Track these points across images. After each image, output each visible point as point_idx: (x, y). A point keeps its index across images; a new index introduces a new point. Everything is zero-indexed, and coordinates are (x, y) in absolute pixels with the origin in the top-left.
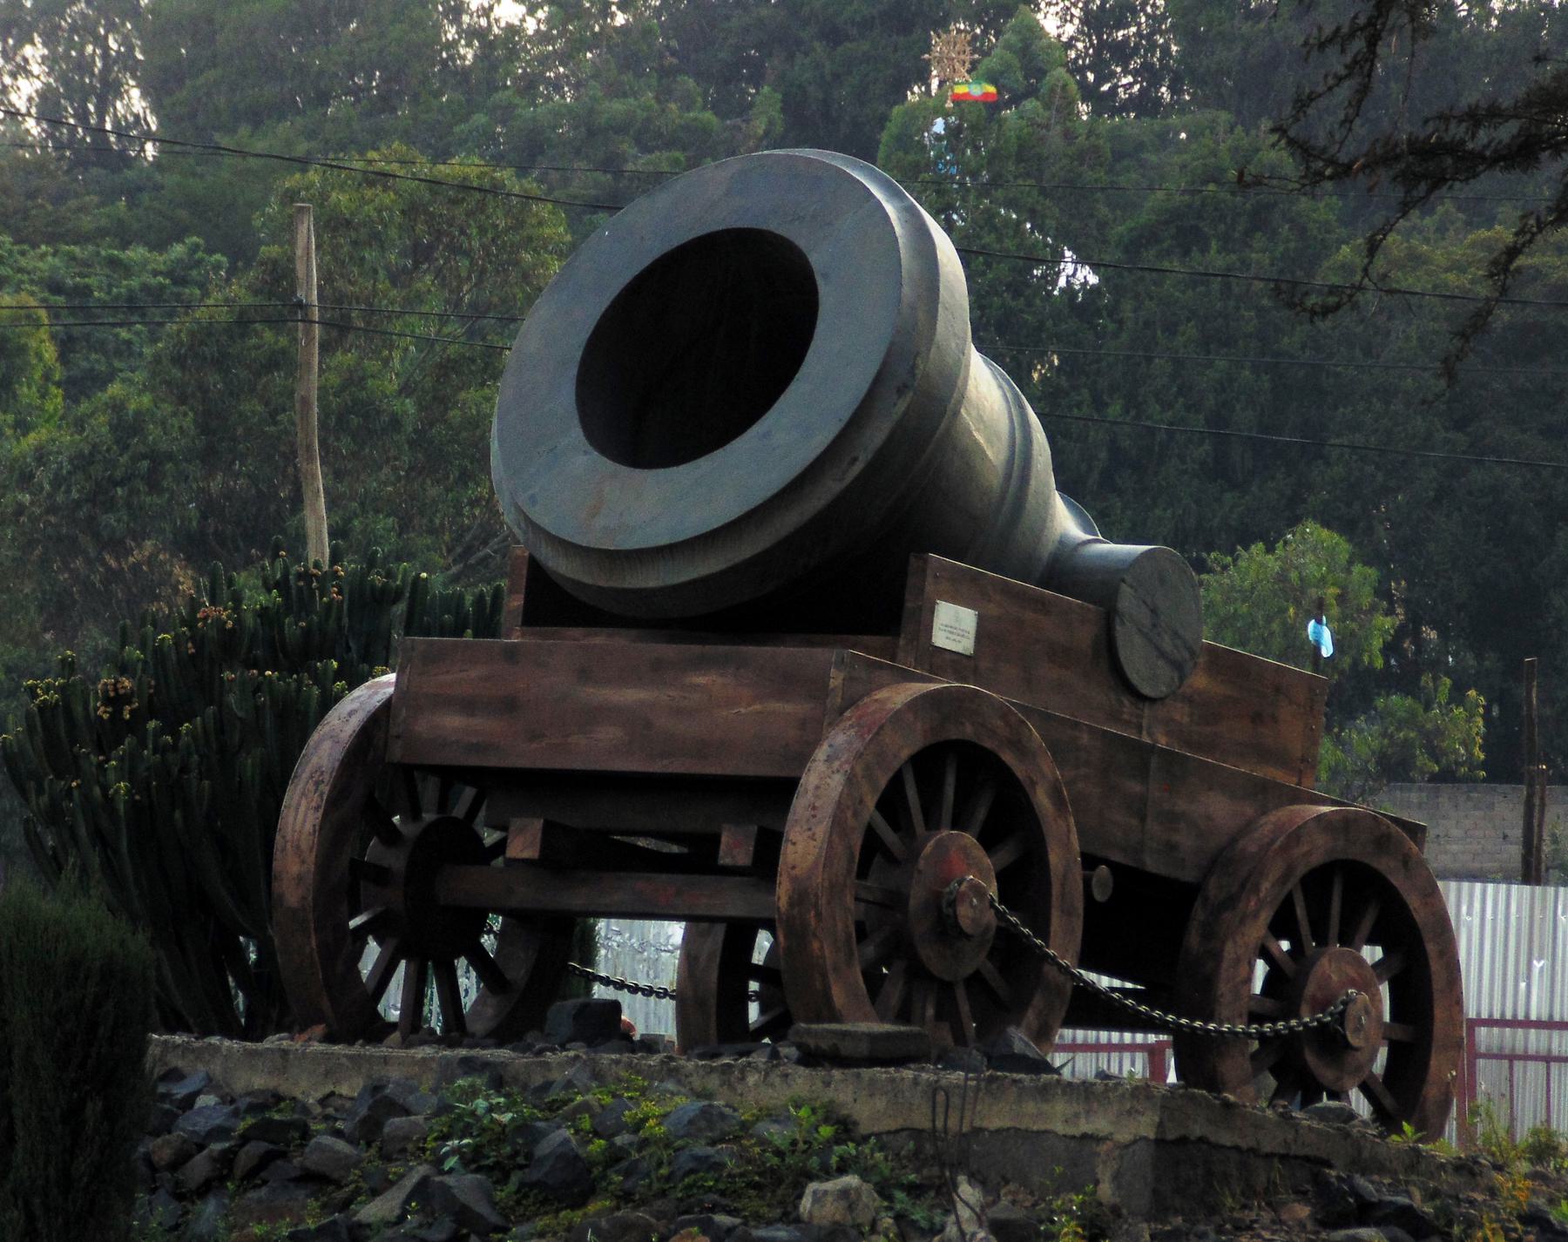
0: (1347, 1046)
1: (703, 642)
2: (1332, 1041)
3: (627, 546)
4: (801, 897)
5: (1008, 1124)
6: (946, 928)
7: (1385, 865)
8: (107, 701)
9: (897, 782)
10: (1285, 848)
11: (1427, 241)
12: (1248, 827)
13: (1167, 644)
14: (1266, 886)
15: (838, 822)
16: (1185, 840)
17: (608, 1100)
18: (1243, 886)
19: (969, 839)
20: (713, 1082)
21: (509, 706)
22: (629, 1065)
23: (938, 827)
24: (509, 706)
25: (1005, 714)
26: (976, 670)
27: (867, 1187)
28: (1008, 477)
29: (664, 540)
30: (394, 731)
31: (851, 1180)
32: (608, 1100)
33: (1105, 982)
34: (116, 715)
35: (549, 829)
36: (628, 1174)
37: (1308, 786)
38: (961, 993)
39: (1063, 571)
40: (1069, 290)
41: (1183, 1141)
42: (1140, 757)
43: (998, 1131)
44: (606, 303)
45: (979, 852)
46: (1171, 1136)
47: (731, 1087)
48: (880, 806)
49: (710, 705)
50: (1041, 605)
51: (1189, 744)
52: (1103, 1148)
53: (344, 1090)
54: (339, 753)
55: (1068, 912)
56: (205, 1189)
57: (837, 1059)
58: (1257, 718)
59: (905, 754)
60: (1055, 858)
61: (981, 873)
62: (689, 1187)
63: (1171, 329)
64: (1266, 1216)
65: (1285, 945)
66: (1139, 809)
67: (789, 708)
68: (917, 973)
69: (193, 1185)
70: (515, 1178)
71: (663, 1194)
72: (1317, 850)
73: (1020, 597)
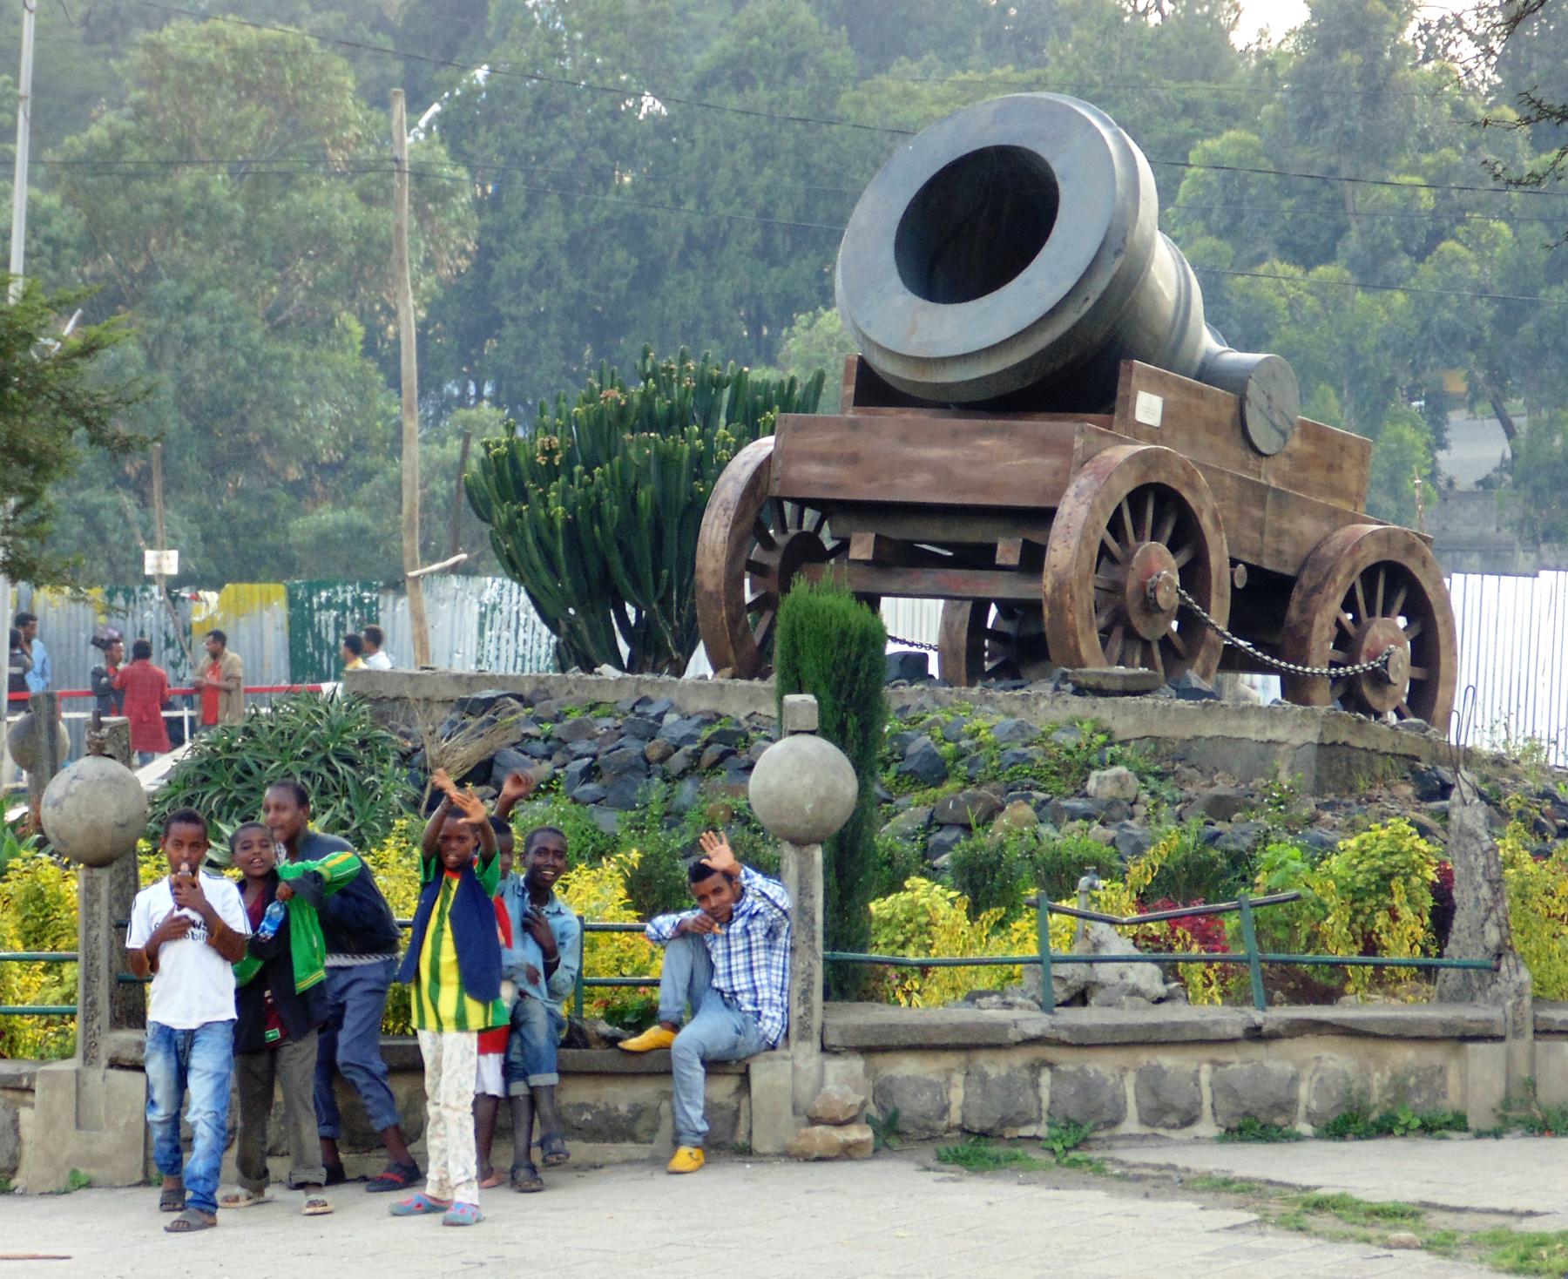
0: (1389, 682)
1: (986, 418)
2: (1379, 678)
3: (935, 355)
4: (1060, 586)
5: (1217, 733)
6: (1150, 606)
7: (1413, 565)
8: (545, 453)
9: (1119, 510)
10: (1352, 553)
11: (915, 81)
12: (1325, 539)
13: (1277, 419)
14: (1340, 578)
15: (1084, 537)
16: (1287, 547)
17: (950, 718)
18: (1326, 578)
19: (1162, 547)
20: (1017, 706)
21: (853, 459)
22: (959, 695)
23: (1142, 539)
24: (853, 459)
25: (1185, 466)
26: (1161, 437)
27: (1131, 774)
28: (1177, 308)
29: (960, 352)
30: (774, 475)
31: (1121, 769)
32: (950, 718)
33: (1241, 642)
34: (550, 462)
35: (879, 539)
36: (970, 765)
37: (1361, 511)
38: (1156, 648)
39: (1208, 373)
40: (648, 116)
41: (1334, 744)
42: (1260, 493)
43: (1210, 739)
44: (913, 195)
45: (1167, 554)
46: (1327, 742)
47: (1029, 710)
48: (1109, 527)
49: (993, 461)
50: (1201, 394)
51: (1290, 485)
52: (1282, 749)
53: (763, 710)
54: (740, 490)
55: (1221, 595)
56: (683, 775)
57: (1099, 692)
58: (1330, 468)
59: (1125, 492)
60: (1214, 560)
61: (1169, 569)
62: (1012, 774)
63: (731, 147)
64: (1385, 793)
65: (1350, 616)
66: (1259, 527)
67: (1047, 461)
68: (1130, 634)
69: (674, 772)
70: (894, 767)
71: (995, 778)
72: (1370, 556)
73: (1188, 388)
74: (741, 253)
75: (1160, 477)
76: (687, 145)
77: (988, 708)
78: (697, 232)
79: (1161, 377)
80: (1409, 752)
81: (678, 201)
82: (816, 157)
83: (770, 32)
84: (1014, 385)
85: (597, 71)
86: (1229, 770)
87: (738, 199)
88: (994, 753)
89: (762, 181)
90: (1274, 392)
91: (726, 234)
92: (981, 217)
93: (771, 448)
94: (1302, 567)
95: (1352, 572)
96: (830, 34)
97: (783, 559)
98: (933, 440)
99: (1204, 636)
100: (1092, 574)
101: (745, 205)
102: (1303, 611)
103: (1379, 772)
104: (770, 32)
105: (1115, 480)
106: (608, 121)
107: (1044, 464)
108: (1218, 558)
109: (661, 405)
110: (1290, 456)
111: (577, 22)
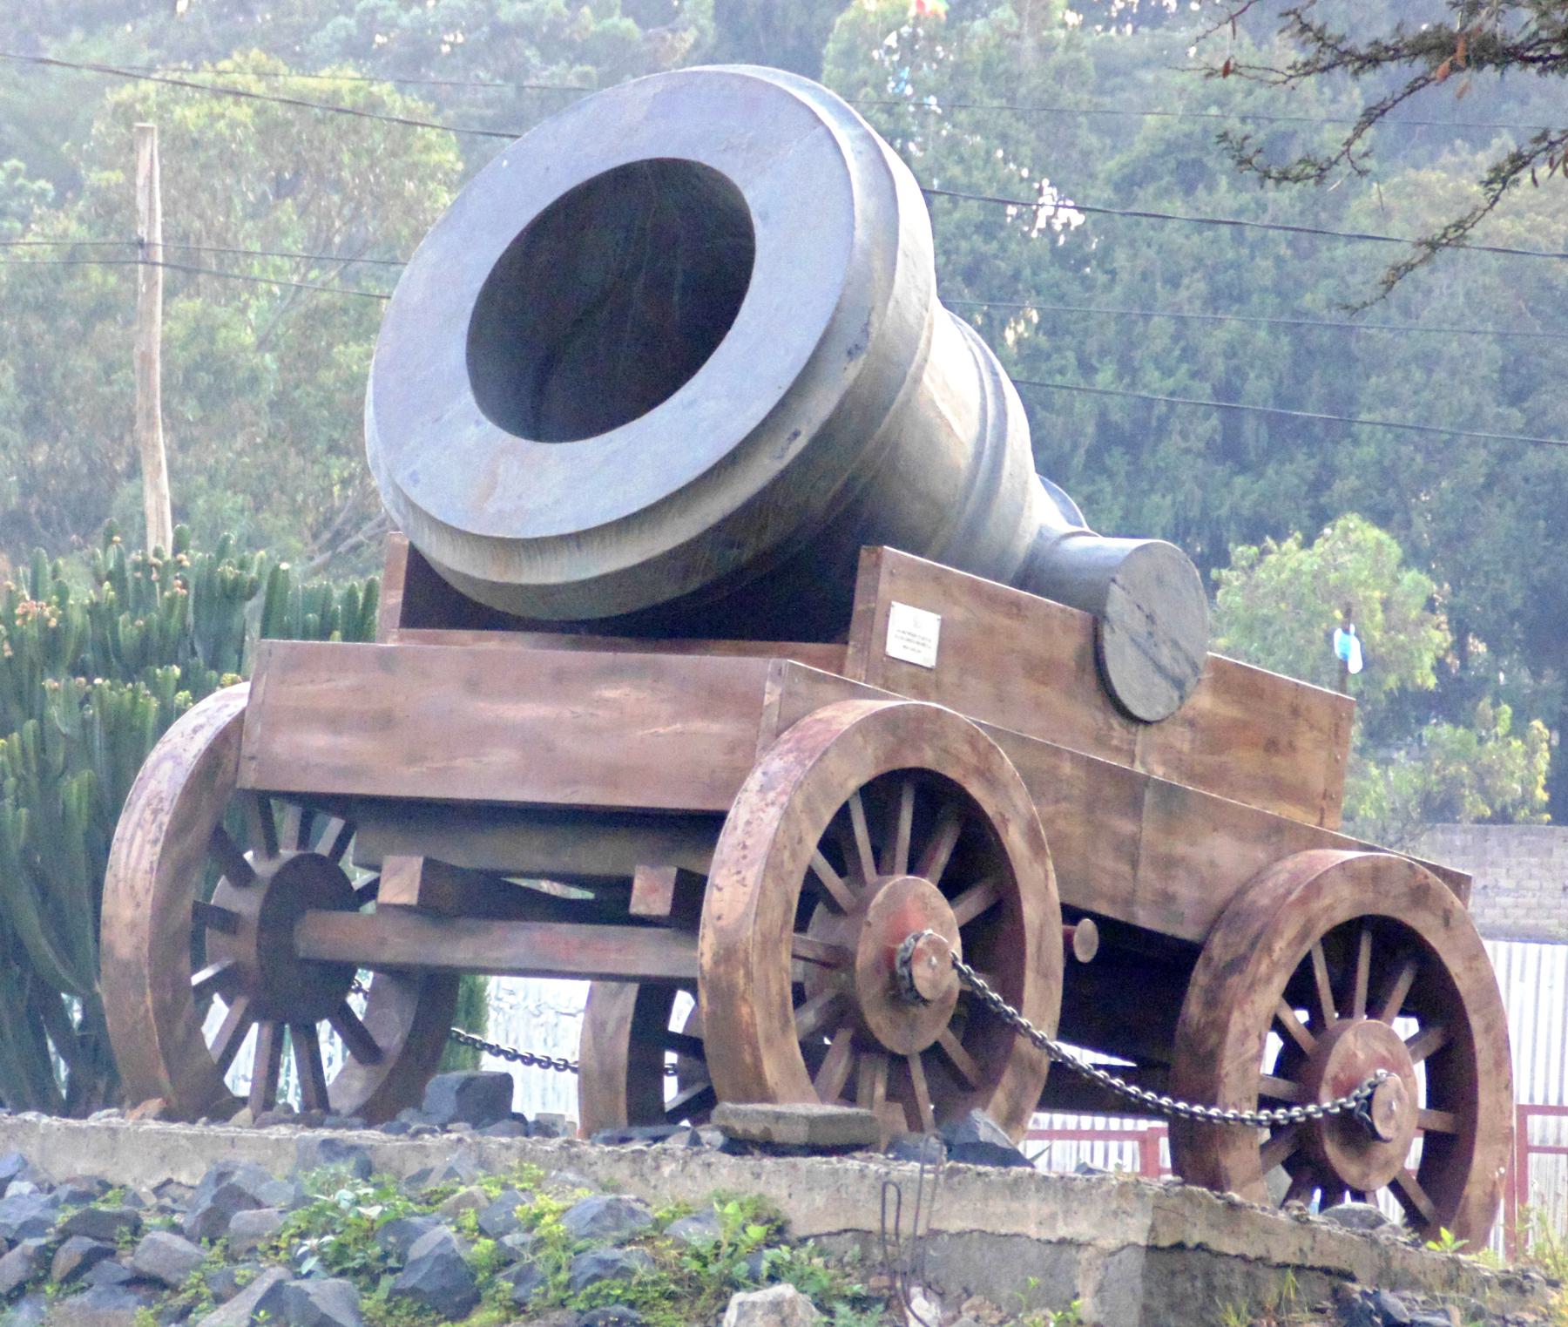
0: (1376, 1136)
2: (1357, 1129)
4: (727, 954)
7: (1424, 924)
9: (844, 813)
10: (1303, 901)
12: (1258, 877)
13: (1165, 655)
14: (1280, 945)
15: (772, 866)
16: (1185, 891)
17: (496, 1192)
18: (1253, 945)
19: (927, 886)
20: (622, 1172)
21: (384, 722)
24: (384, 722)
25: (972, 740)
26: (938, 685)
27: (805, 1298)
30: (248, 749)
31: (785, 1290)
35: (430, 866)
36: (519, 1279)
38: (917, 1070)
39: (1038, 575)
41: (1180, 1247)
42: (1131, 790)
43: (960, 1234)
45: (938, 899)
52: (1084, 1256)
53: (184, 1177)
54: (182, 778)
55: (1044, 974)
57: (772, 1148)
58: (1272, 746)
59: (854, 783)
62: (592, 1297)
63: (1174, 282)
65: (1303, 1016)
66: (1130, 851)
67: (715, 728)
68: (864, 1044)
70: (387, 1282)
71: (562, 1304)
72: (1342, 905)
74: (1187, 451)
75: (926, 758)
76: (1102, 278)
77: (571, 1176)
78: (1116, 416)
79: (938, 577)
80: (1332, 1263)
81: (1087, 369)
82: (1307, 300)
83: (1239, 97)
84: (669, 591)
85: (962, 160)
86: (989, 1294)
87: (1185, 367)
88: (564, 1258)
89: (1221, 335)
90: (1160, 611)
91: (1164, 421)
92: (622, 284)
93: (242, 703)
94: (1212, 927)
95: (1303, 936)
96: (1334, 100)
97: (268, 899)
98: (521, 690)
99: (1010, 1046)
100: (789, 932)
101: (1194, 375)
102: (1211, 1002)
103: (1271, 1299)
104: (1239, 97)
105: (833, 763)
106: (977, 240)
107: (712, 732)
108: (1038, 910)
109: (128, 628)
110: (1192, 723)
111: (931, 82)
